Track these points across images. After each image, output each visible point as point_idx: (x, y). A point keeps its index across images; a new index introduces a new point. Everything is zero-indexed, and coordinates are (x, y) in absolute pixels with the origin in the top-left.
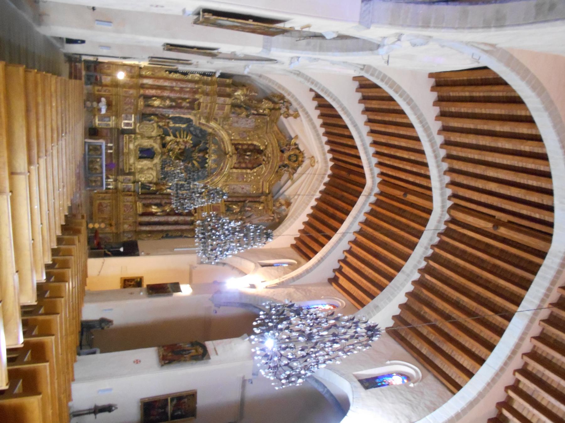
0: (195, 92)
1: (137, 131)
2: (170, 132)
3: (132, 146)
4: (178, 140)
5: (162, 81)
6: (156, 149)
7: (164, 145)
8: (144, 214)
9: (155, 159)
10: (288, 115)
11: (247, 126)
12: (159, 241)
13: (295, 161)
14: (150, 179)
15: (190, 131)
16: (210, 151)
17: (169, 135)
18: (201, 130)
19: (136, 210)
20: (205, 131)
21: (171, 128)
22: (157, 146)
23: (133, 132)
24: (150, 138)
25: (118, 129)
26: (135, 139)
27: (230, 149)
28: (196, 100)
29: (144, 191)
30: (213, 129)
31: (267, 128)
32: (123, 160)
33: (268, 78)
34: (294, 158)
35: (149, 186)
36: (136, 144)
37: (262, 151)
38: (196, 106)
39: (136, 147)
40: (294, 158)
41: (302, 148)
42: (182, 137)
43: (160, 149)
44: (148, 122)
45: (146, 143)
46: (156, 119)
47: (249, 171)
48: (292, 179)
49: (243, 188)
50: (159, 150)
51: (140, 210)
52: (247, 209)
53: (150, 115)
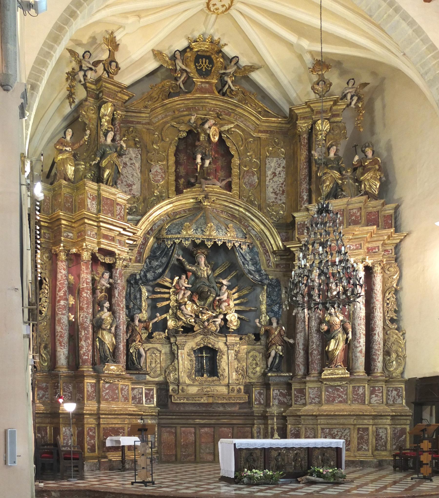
0: (74, 259)
1: (161, 379)
2: (159, 317)
3: (191, 386)
4: (172, 303)
5: (58, 329)
6: (197, 344)
7: (188, 330)
8: (348, 363)
9: (216, 346)
10: (111, 66)
11: (138, 165)
12: (407, 336)
13: (211, 62)
14: (259, 357)
15: (155, 279)
16: (199, 237)
17: (165, 321)
18: (153, 256)
19: (341, 379)
20: (153, 251)
21: (151, 318)
22: (192, 343)
23: (163, 387)
24: (173, 356)
25: (159, 413)
26: (178, 382)
27: (187, 200)
28: (94, 259)
29: (284, 367)
30: (148, 233)
31: (139, 123)
32: (223, 404)
33: (33, 68)
34: (204, 64)
35: (275, 358)
36: (188, 381)
37: (190, 132)
38: (108, 260)
39: (194, 380)
40: (204, 64)
41: (182, 44)
42: (166, 296)
43: (195, 337)
44: (143, 360)
45: (185, 361)
46: (137, 344)
47: (236, 161)
48: (252, 68)
49: (274, 174)
50: (199, 339)
51: (341, 372)
52: (332, 155)
53: (128, 354)
